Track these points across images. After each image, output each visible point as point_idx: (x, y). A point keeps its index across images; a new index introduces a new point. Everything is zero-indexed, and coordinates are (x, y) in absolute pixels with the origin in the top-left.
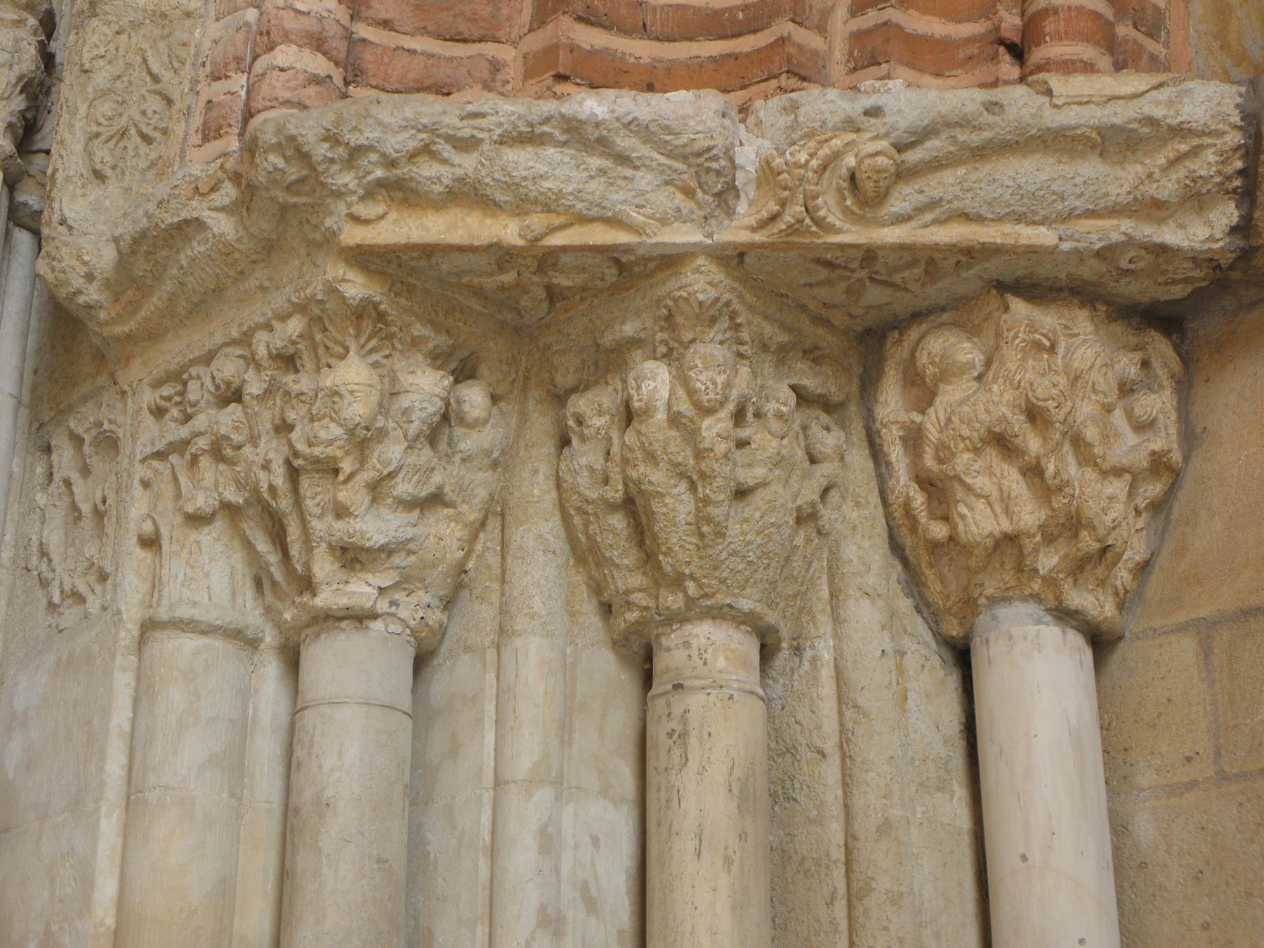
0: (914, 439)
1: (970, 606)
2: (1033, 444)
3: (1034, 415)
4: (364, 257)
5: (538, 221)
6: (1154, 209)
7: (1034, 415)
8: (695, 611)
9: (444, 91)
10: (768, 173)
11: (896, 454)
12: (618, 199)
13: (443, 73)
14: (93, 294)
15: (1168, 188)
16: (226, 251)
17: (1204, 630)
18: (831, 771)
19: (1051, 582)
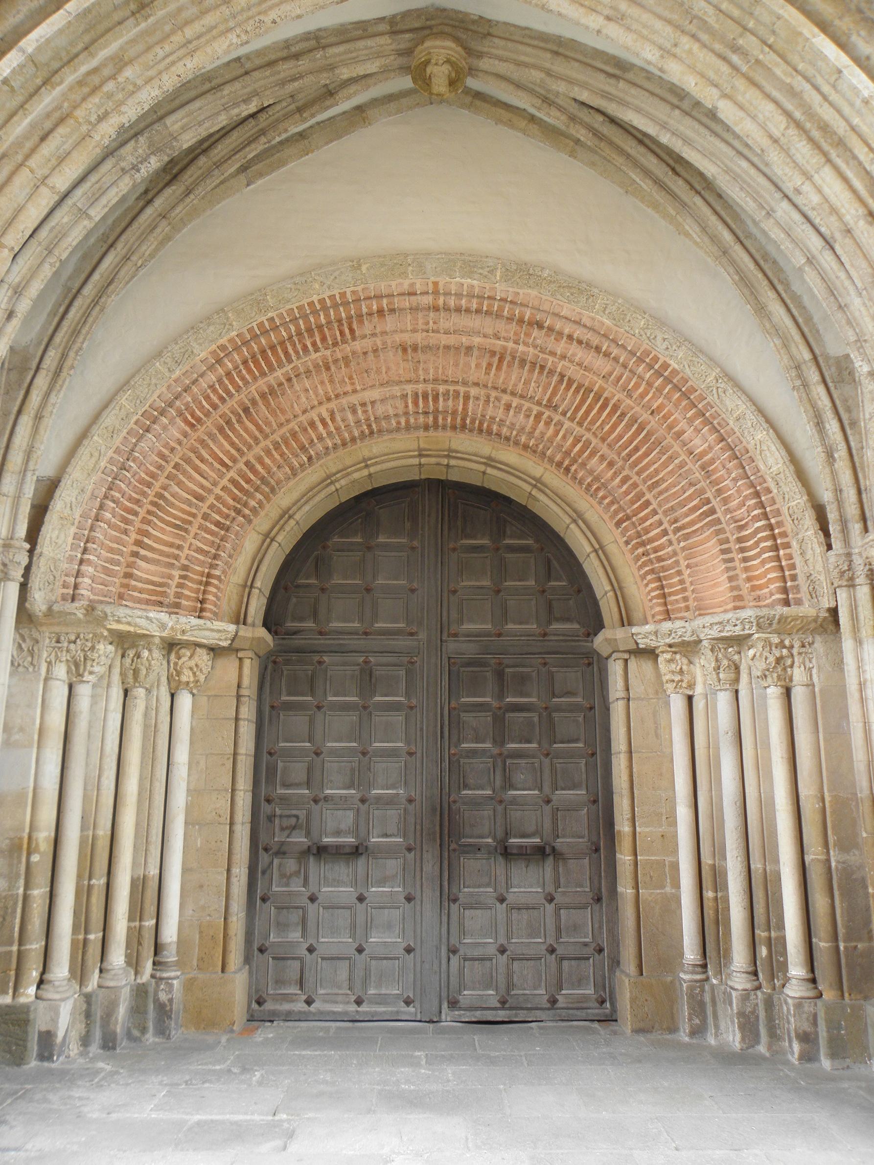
0: (176, 664)
1: (177, 688)
2: (195, 669)
3: (196, 665)
4: (109, 630)
5: (137, 628)
6: (220, 640)
7: (196, 665)
8: (140, 686)
9: (106, 586)
10: (172, 628)
11: (172, 665)
12: (149, 627)
13: (106, 583)
14: (40, 614)
15: (223, 638)
16: (79, 620)
17: (209, 697)
18: (154, 712)
19: (191, 688)
